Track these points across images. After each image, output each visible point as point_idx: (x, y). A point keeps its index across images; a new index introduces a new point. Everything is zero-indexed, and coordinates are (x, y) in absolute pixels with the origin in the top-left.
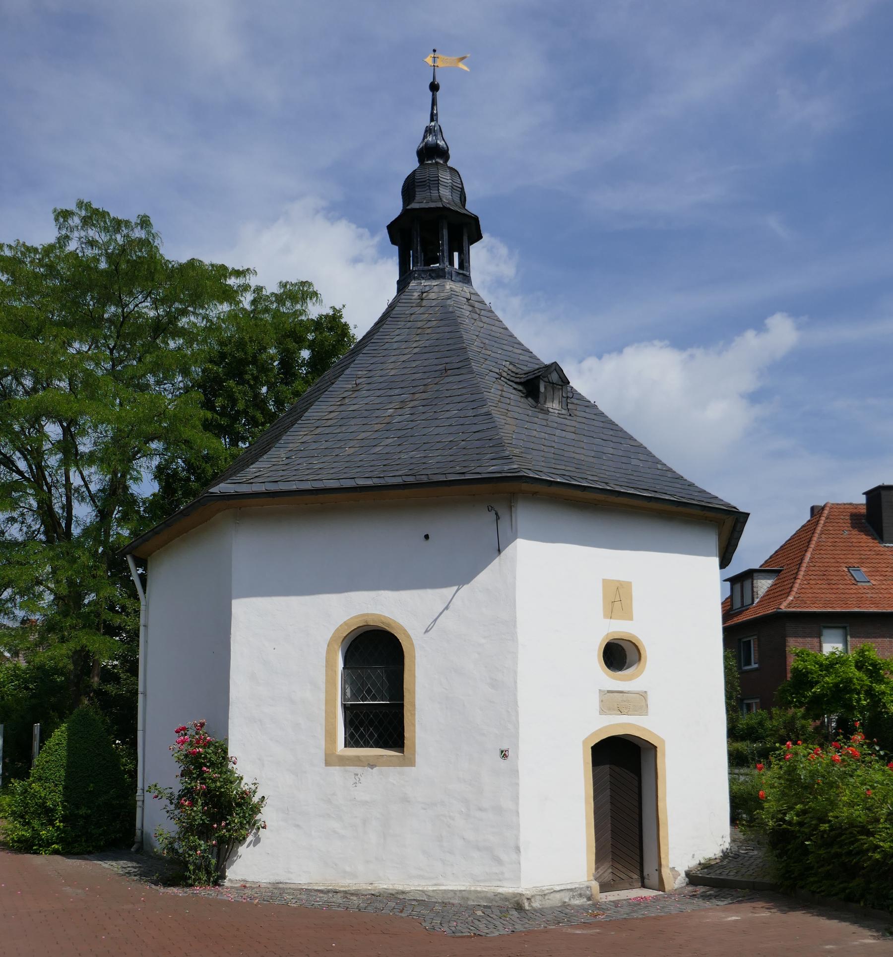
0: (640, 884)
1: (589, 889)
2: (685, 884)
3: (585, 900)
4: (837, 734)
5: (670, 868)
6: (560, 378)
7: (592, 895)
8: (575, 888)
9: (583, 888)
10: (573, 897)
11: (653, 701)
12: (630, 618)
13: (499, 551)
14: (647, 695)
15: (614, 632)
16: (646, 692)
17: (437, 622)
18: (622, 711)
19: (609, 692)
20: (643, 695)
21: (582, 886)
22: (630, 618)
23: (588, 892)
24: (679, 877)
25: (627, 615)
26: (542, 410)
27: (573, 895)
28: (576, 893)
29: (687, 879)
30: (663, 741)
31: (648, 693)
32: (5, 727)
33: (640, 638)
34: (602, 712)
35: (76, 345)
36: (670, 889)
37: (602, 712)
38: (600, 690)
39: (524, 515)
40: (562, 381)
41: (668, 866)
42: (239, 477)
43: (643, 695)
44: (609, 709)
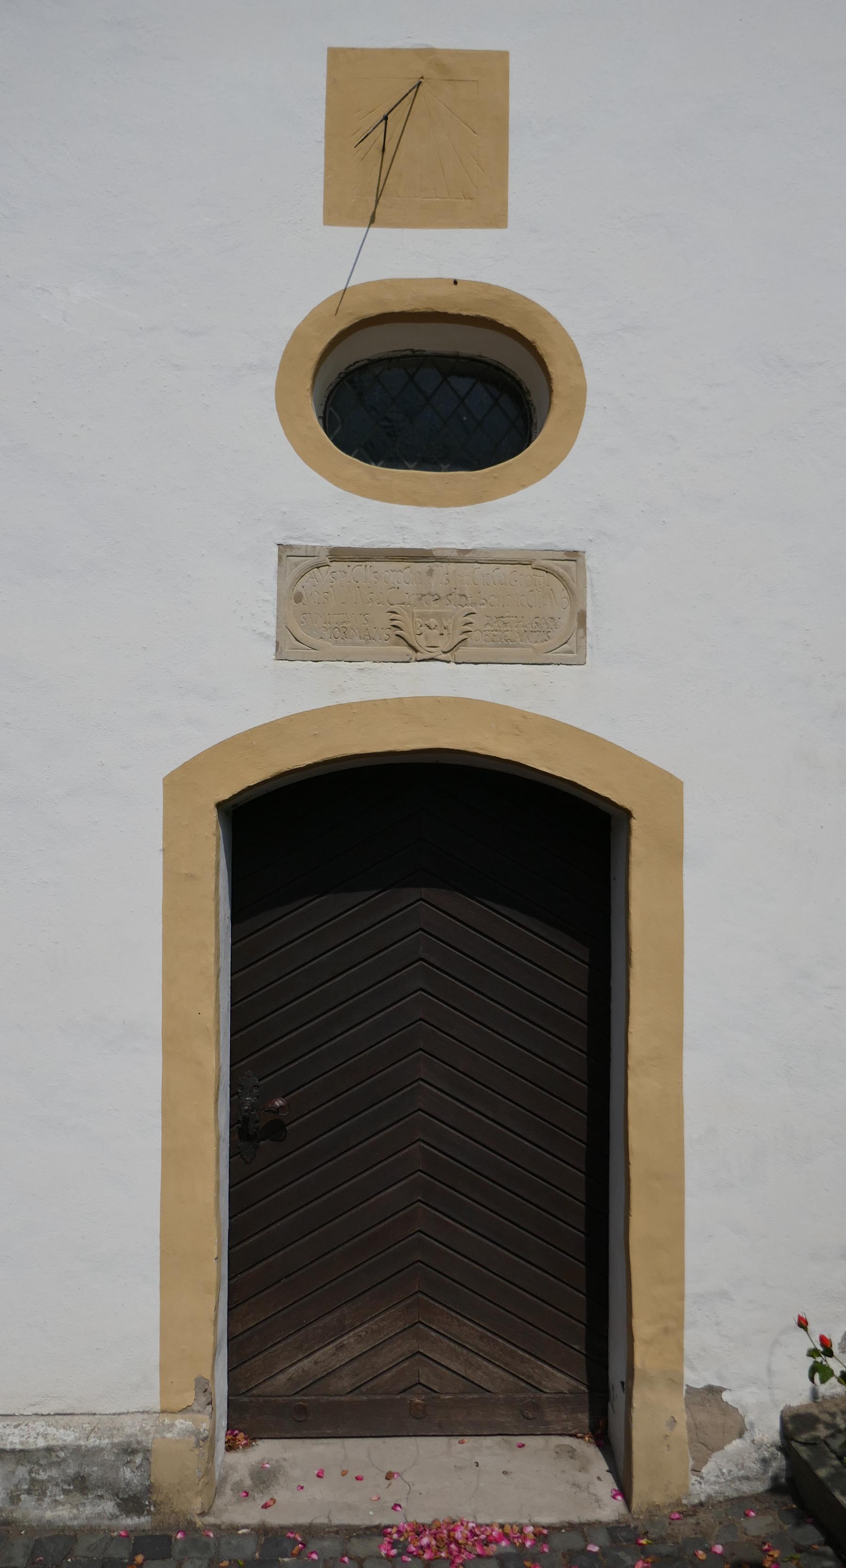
0: (584, 1418)
1: (138, 1459)
2: (760, 1487)
3: (109, 1506)
4: (174, 1531)
5: (691, 1391)
7: (149, 1489)
8: (49, 1450)
9: (99, 1450)
10: (37, 1489)
14: (582, 568)
16: (573, 556)
17: (375, 198)
18: (421, 642)
19: (338, 555)
21: (93, 1442)
23: (127, 1473)
24: (736, 1444)
27: (33, 1481)
28: (54, 1472)
29: (779, 1463)
31: (590, 562)
33: (292, 321)
36: (658, 1498)
41: (675, 1381)
44: (342, 633)
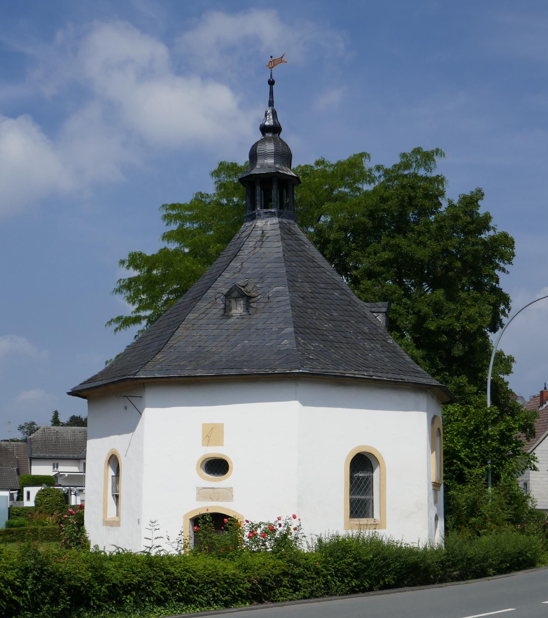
6: (239, 293)
11: (236, 492)
12: (222, 445)
13: (141, 414)
15: (209, 454)
16: (232, 488)
18: (213, 499)
19: (203, 488)
20: (230, 490)
22: (222, 445)
25: (220, 442)
26: (227, 316)
30: (185, 516)
31: (234, 489)
32: (33, 507)
33: (228, 455)
34: (198, 499)
35: (322, 219)
37: (198, 499)
38: (197, 487)
39: (149, 395)
40: (241, 295)
42: (149, 366)
43: (230, 490)
